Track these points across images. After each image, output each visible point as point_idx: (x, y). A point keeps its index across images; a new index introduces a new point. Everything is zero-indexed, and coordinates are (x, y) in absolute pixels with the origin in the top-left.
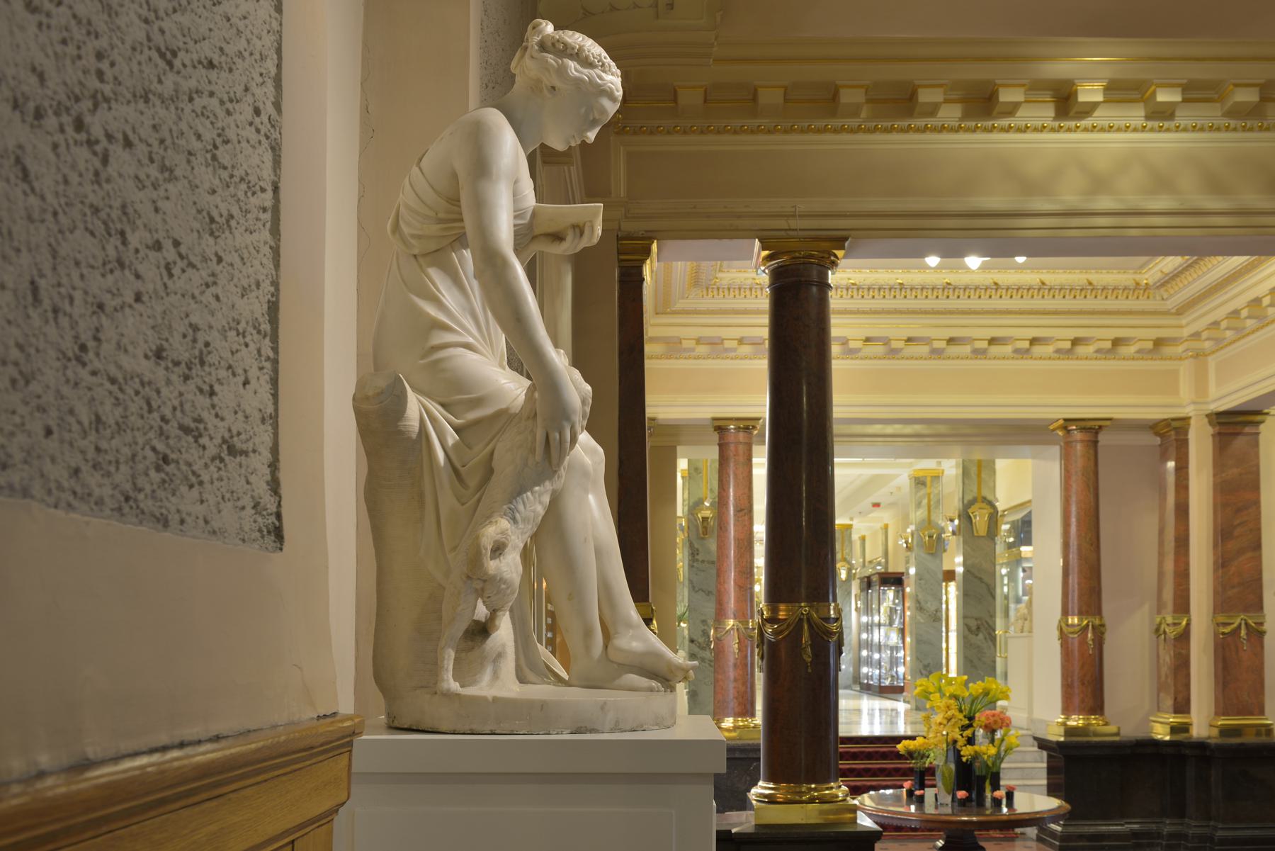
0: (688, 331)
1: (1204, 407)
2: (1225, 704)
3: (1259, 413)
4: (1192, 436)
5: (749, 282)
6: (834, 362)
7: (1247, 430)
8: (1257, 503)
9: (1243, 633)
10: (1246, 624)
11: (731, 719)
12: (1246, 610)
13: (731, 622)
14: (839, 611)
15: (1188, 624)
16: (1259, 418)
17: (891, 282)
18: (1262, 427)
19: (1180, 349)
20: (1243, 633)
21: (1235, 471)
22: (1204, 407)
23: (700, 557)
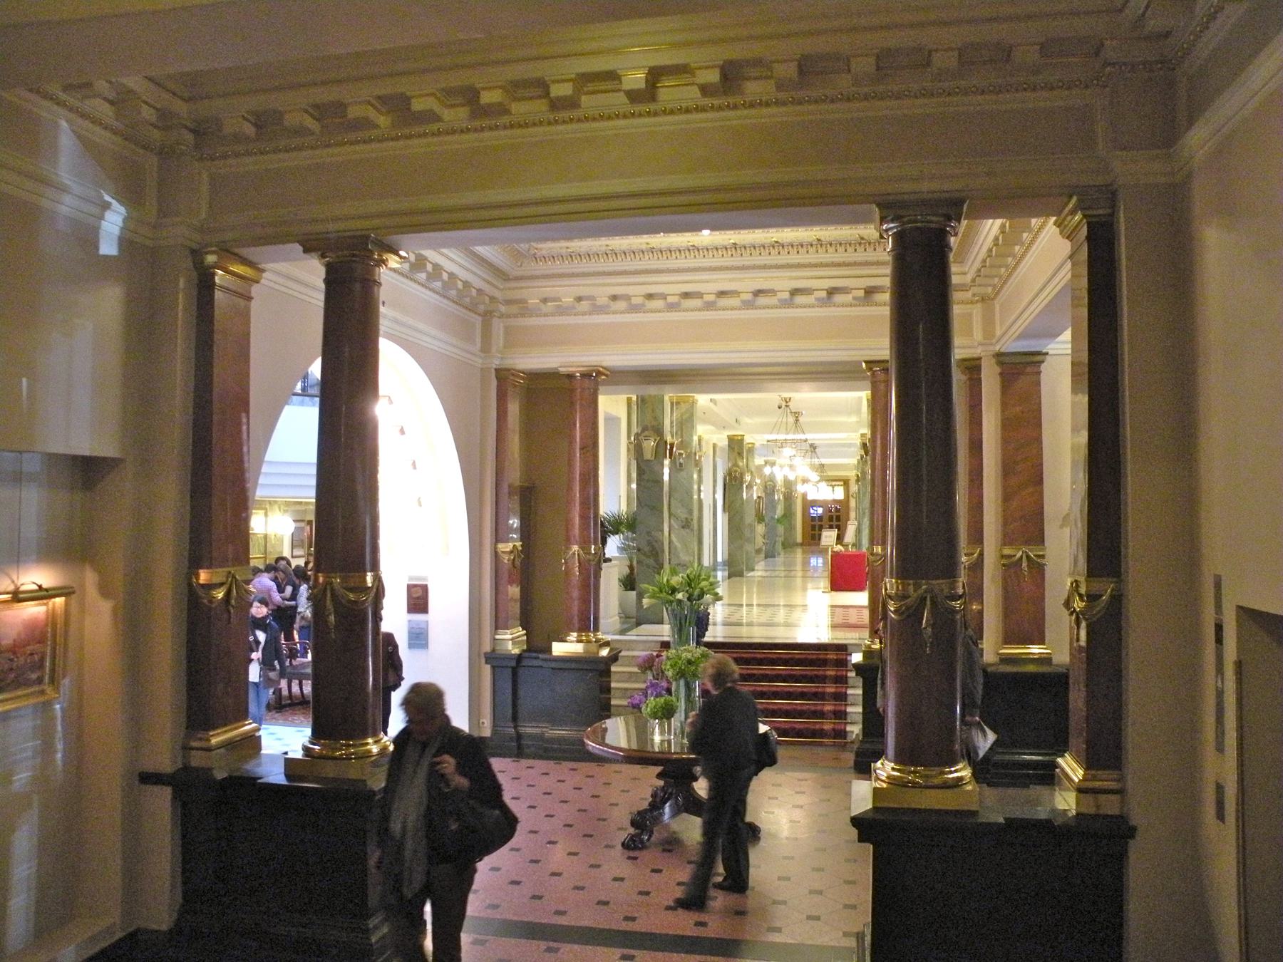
0: (566, 292)
1: (991, 348)
2: (1012, 635)
3: (1039, 353)
4: (984, 375)
5: (604, 248)
6: (955, 307)
7: (1029, 369)
8: (1038, 440)
9: (1024, 564)
10: (1028, 557)
11: (575, 634)
12: (1027, 543)
13: (575, 548)
14: (378, 579)
15: (981, 554)
16: (1038, 358)
17: (726, 243)
18: (1043, 367)
19: (969, 295)
20: (1024, 564)
21: (1018, 409)
22: (991, 348)
23: (645, 477)
